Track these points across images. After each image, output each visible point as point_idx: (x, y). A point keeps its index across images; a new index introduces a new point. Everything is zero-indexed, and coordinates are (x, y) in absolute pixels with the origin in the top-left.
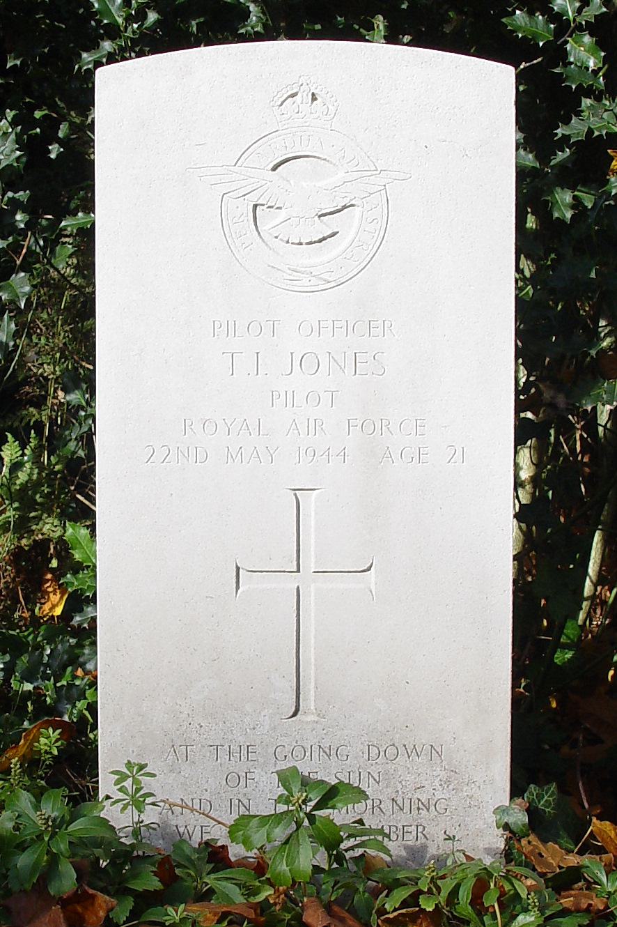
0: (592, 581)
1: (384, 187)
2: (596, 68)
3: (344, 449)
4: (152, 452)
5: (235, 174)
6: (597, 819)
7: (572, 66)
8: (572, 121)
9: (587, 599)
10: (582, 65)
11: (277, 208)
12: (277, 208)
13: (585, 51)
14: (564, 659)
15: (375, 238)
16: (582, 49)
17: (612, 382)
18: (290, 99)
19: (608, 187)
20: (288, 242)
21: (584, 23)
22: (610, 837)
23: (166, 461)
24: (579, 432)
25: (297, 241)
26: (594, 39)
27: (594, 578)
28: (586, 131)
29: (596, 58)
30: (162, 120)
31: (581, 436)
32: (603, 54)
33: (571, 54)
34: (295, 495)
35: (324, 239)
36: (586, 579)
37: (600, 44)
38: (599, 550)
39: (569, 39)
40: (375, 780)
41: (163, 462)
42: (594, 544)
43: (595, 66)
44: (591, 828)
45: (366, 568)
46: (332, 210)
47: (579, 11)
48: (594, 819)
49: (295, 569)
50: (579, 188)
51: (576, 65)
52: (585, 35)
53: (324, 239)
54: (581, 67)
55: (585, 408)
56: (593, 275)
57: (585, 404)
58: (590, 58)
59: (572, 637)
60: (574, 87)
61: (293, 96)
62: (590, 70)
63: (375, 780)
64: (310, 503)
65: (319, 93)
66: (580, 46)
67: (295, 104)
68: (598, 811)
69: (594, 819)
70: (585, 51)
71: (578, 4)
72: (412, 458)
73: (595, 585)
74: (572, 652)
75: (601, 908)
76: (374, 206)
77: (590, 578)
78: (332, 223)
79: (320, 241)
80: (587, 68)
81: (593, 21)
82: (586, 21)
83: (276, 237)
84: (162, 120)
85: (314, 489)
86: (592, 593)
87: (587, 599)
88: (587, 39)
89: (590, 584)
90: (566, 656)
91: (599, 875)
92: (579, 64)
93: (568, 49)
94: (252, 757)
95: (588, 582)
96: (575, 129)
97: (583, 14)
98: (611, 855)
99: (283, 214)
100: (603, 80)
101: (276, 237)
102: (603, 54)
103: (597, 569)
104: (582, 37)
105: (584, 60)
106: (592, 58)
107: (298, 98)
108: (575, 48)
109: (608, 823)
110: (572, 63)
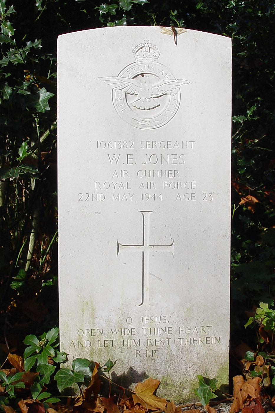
0: (30, 253)
1: (178, 86)
2: (12, 36)
3: (161, 194)
4: (81, 196)
5: (117, 80)
6: (11, 354)
7: (2, 35)
8: (3, 58)
9: (28, 260)
10: (6, 34)
11: (135, 95)
12: (135, 95)
13: (7, 28)
14: (18, 286)
15: (175, 107)
16: (6, 27)
17: (14, 169)
18: (140, 50)
19: (23, 86)
20: (139, 109)
21: (6, 17)
22: (16, 361)
23: (81, 200)
24: (24, 190)
25: (144, 108)
26: (11, 23)
27: (31, 251)
28: (8, 62)
29: (12, 32)
30: (89, 61)
31: (25, 191)
32: (14, 30)
33: (2, 30)
34: (142, 213)
35: (155, 107)
36: (28, 252)
37: (13, 26)
38: (33, 239)
39: (2, 23)
40: (101, 333)
41: (86, 200)
42: (31, 237)
43: (11, 35)
44: (8, 357)
45: (171, 244)
46: (158, 96)
47: (6, 11)
48: (10, 354)
49: (142, 245)
50: (15, 86)
51: (4, 34)
52: (8, 21)
53: (155, 107)
54: (6, 35)
55: (2, 180)
56: (6, 124)
57: (3, 178)
58: (9, 31)
59: (22, 276)
60: (2, 43)
61: (141, 48)
62: (9, 36)
63: (101, 333)
64: (148, 216)
65: (152, 47)
66: (5, 26)
67: (155, 53)
68: (15, 350)
69: (10, 354)
70: (7, 28)
71: (5, 9)
72: (189, 198)
73: (32, 254)
74: (22, 283)
75: (3, 391)
76: (174, 94)
77: (30, 251)
78: (158, 101)
79: (152, 109)
80: (8, 36)
81: (9, 16)
82: (7, 16)
83: (135, 107)
84: (89, 61)
85: (150, 212)
86: (31, 257)
87: (28, 260)
88: (9, 23)
89: (30, 254)
90: (19, 285)
91: (4, 377)
92: (5, 34)
93: (1, 27)
94: (146, 321)
95: (29, 253)
96: (4, 61)
97: (7, 13)
98: (15, 368)
99: (137, 98)
100: (15, 41)
101: (135, 107)
102: (14, 30)
103: (32, 247)
104: (6, 23)
105: (7, 32)
106: (10, 31)
107: (143, 49)
108: (4, 27)
109: (15, 355)
110: (2, 33)
